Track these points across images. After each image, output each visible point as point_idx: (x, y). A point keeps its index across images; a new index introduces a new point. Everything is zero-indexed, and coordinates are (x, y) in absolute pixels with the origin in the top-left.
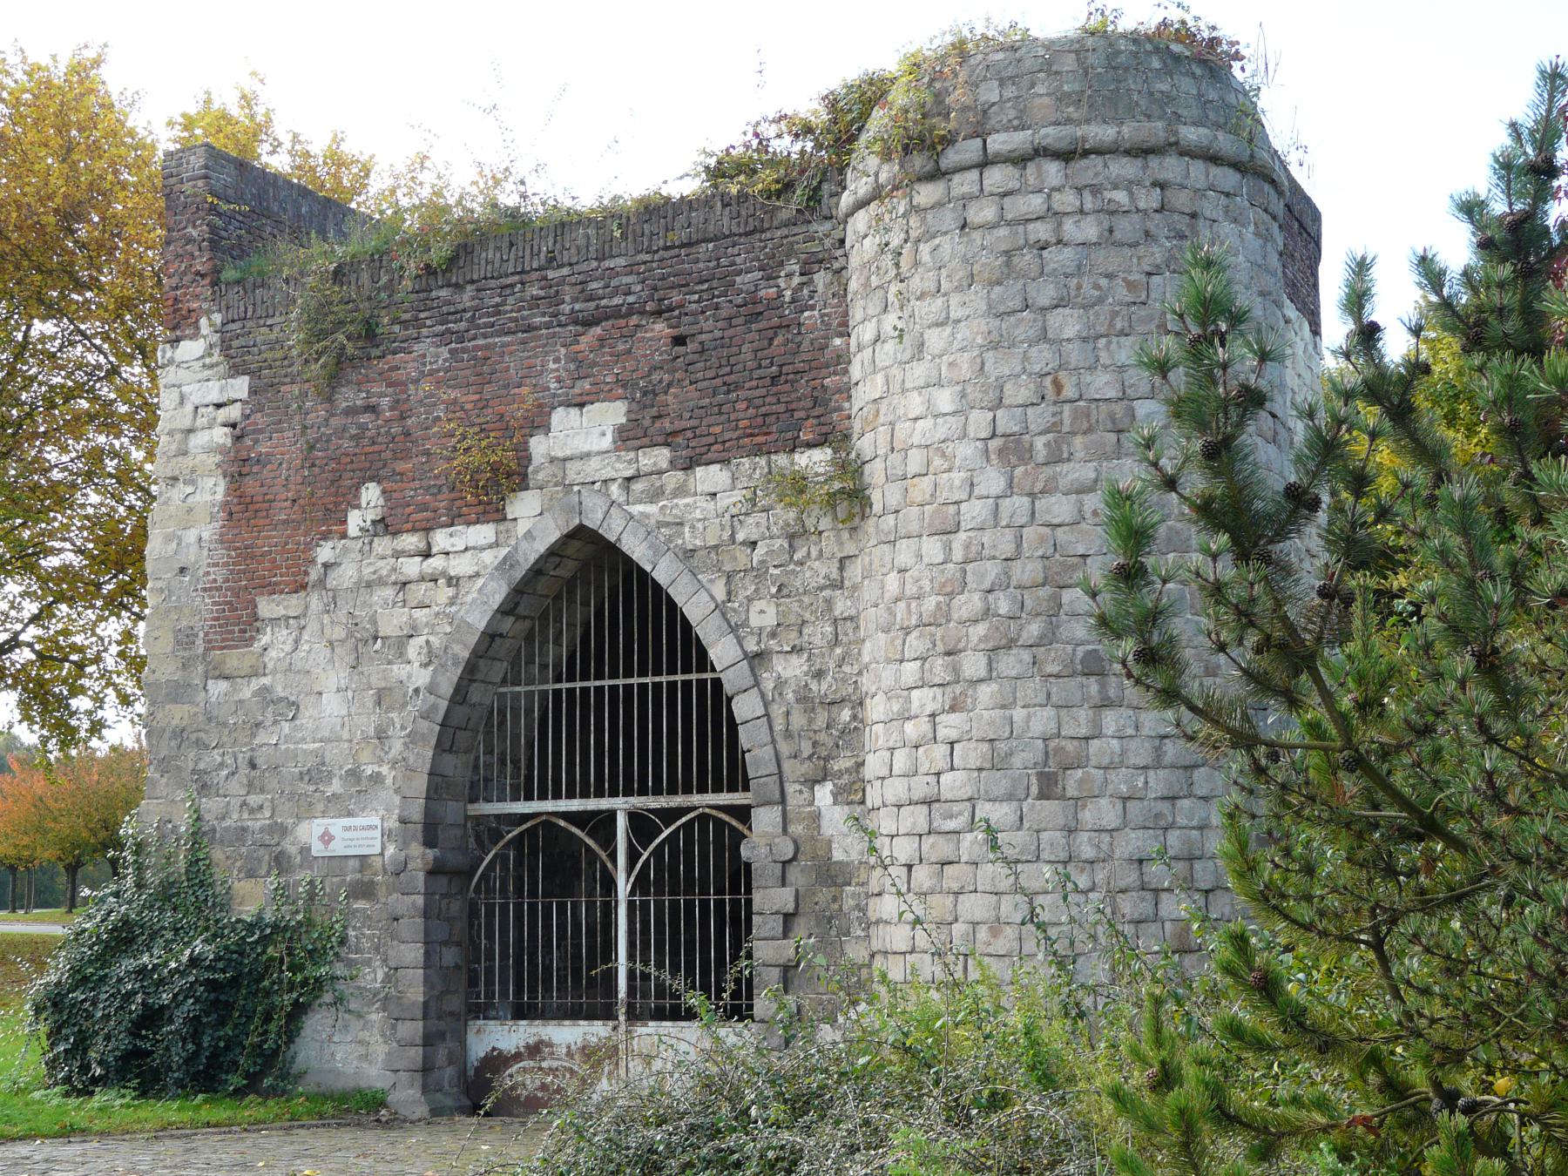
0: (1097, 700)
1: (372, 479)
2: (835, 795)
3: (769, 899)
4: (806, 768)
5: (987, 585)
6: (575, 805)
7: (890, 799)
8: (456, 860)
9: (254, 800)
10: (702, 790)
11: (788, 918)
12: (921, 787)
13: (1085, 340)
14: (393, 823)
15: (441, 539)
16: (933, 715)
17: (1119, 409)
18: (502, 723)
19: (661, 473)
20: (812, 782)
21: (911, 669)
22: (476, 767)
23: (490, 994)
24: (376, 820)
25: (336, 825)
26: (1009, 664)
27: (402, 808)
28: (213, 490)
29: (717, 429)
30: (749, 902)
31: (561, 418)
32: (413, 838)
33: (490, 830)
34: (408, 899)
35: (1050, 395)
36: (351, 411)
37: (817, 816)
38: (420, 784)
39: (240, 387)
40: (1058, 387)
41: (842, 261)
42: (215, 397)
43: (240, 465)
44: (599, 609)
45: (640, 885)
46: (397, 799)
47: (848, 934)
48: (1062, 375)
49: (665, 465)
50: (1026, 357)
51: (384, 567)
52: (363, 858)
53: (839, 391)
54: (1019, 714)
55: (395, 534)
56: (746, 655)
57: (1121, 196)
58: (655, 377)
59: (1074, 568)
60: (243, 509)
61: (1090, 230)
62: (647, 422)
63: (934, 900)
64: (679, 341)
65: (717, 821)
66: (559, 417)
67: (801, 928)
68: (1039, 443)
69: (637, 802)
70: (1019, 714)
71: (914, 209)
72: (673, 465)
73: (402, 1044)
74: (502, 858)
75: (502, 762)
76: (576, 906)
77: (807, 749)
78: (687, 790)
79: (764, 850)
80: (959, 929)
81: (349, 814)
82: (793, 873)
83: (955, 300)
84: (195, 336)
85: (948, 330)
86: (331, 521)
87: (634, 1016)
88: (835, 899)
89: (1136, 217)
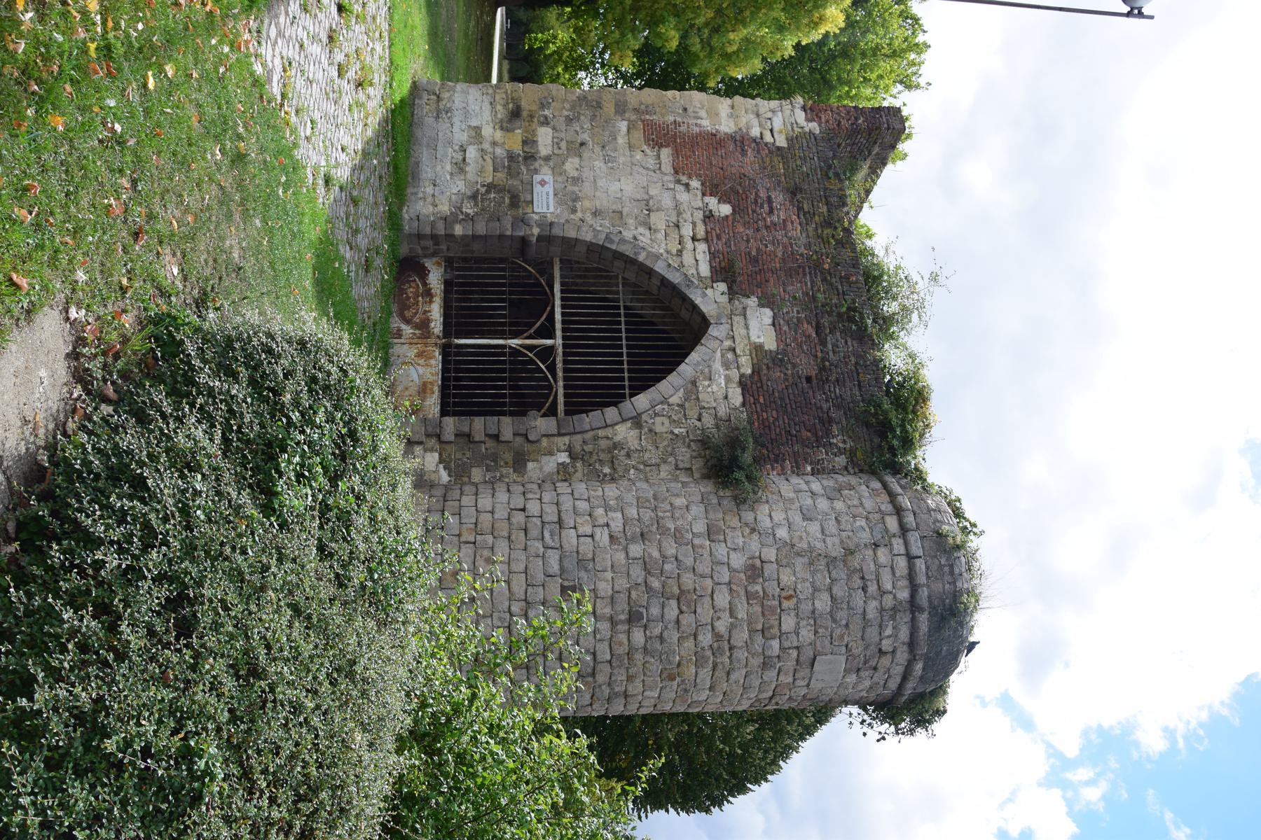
0: (615, 618)
1: (734, 210)
2: (563, 464)
3: (507, 426)
4: (578, 448)
5: (680, 557)
6: (558, 317)
7: (562, 498)
8: (532, 252)
9: (563, 145)
10: (565, 387)
11: (496, 437)
12: (569, 520)
13: (813, 612)
14: (550, 218)
15: (702, 247)
16: (608, 525)
17: (775, 631)
18: (601, 277)
19: (738, 368)
20: (570, 450)
21: (632, 512)
22: (578, 263)
23: (458, 269)
24: (552, 209)
25: (549, 188)
26: (637, 573)
27: (558, 223)
28: (726, 126)
29: (762, 400)
30: (503, 414)
31: (768, 313)
32: (542, 230)
33: (545, 267)
34: (509, 226)
35: (784, 594)
36: (769, 199)
37: (551, 454)
38: (572, 234)
39: (781, 142)
40: (788, 598)
41: (852, 471)
42: (776, 129)
43: (741, 141)
44: (659, 330)
45: (515, 352)
46: (562, 221)
47: (488, 470)
48: (795, 600)
49: (742, 371)
50: (804, 580)
51: (687, 216)
52: (532, 202)
53: (783, 469)
54: (609, 575)
55: (704, 221)
56: (639, 415)
57: (889, 632)
58: (789, 366)
59: (689, 607)
60: (714, 141)
61: (872, 613)
62: (765, 361)
63: (505, 525)
64: (809, 379)
65: (549, 395)
66: (768, 313)
67: (490, 443)
68: (758, 588)
69: (560, 350)
70: (609, 575)
71: (883, 514)
72: (742, 376)
73: (433, 227)
74: (530, 275)
75: (580, 277)
76: (504, 316)
77: (588, 448)
78: (565, 379)
79: (533, 424)
80: (490, 539)
81: (555, 195)
82: (519, 440)
83: (836, 540)
84: (808, 120)
85: (819, 536)
86: (711, 188)
87: (446, 351)
88: (506, 463)
89: (877, 639)
